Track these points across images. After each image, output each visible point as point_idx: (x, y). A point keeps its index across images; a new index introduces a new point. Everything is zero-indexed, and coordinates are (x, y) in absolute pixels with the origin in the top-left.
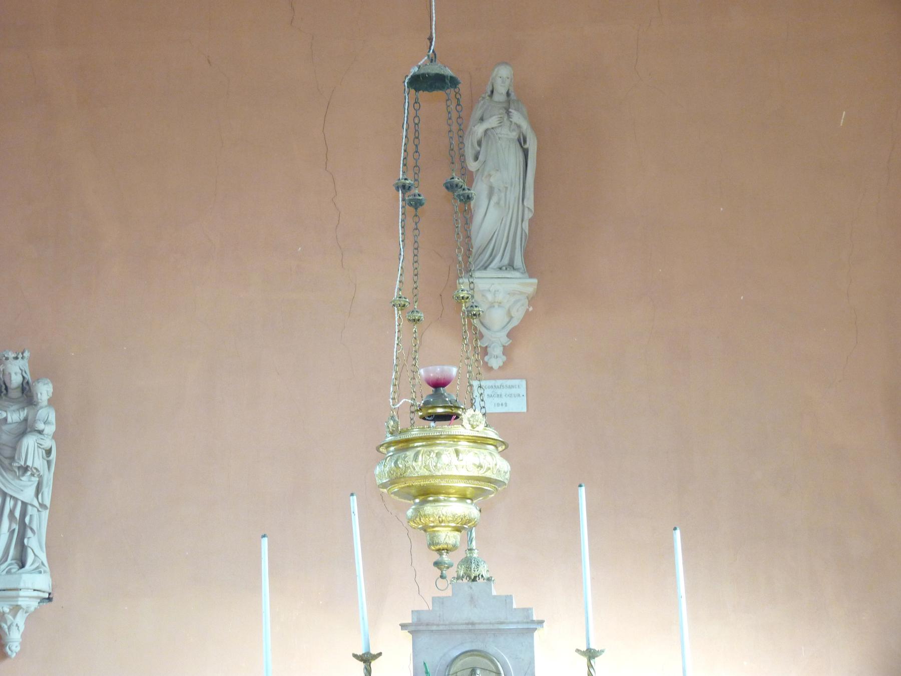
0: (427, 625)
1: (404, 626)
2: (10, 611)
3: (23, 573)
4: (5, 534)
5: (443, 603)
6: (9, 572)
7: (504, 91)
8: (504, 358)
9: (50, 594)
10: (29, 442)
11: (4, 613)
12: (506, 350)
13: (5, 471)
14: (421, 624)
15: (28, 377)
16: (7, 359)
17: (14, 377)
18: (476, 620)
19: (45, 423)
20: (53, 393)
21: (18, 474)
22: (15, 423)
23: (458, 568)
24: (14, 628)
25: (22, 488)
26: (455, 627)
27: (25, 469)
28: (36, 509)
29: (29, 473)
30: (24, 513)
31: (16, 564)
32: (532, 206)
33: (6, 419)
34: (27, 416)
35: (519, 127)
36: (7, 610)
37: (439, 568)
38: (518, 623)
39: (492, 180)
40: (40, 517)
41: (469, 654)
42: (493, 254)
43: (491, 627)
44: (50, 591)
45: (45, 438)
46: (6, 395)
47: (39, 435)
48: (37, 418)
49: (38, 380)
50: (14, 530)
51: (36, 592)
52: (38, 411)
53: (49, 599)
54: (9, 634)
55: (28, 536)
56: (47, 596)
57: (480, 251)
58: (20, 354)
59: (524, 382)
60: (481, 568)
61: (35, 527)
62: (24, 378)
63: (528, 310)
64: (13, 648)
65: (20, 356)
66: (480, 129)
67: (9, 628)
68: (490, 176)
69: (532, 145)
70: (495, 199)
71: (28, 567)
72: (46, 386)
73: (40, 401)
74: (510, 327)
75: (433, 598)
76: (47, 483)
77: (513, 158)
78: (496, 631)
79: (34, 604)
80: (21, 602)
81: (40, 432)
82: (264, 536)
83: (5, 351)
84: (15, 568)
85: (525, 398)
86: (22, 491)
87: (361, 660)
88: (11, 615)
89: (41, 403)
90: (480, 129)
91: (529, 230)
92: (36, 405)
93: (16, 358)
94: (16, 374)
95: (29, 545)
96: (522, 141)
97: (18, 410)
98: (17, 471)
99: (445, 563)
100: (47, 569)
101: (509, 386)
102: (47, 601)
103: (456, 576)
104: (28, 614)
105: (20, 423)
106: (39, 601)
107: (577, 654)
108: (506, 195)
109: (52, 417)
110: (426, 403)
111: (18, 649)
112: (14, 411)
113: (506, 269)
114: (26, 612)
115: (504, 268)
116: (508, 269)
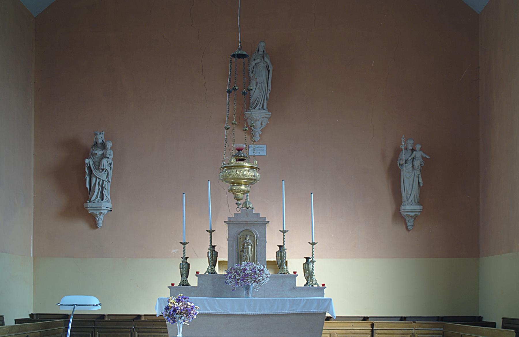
0: (233, 221)
1: (225, 222)
2: (99, 213)
3: (103, 202)
6: (98, 202)
7: (262, 51)
8: (260, 138)
9: (111, 209)
10: (104, 161)
11: (97, 214)
12: (260, 135)
13: (97, 170)
14: (231, 221)
15: (104, 140)
16: (97, 134)
17: (99, 140)
18: (248, 221)
19: (109, 155)
20: (112, 145)
24: (100, 219)
27: (103, 169)
29: (104, 171)
33: (97, 153)
34: (104, 153)
35: (267, 62)
36: (98, 213)
38: (261, 222)
39: (257, 80)
42: (257, 104)
43: (252, 223)
46: (97, 146)
50: (100, 189)
53: (111, 211)
56: (110, 209)
59: (266, 146)
61: (106, 188)
62: (102, 140)
63: (267, 123)
64: (100, 225)
65: (101, 133)
66: (254, 63)
67: (98, 219)
68: (256, 78)
69: (271, 69)
70: (258, 86)
71: (104, 200)
72: (110, 143)
77: (265, 73)
78: (254, 224)
79: (106, 212)
81: (108, 158)
84: (100, 201)
85: (266, 151)
86: (102, 176)
90: (254, 63)
93: (100, 134)
94: (100, 139)
96: (268, 67)
97: (101, 151)
98: (100, 170)
100: (110, 201)
105: (101, 155)
106: (108, 211)
109: (112, 153)
111: (101, 225)
113: (261, 109)
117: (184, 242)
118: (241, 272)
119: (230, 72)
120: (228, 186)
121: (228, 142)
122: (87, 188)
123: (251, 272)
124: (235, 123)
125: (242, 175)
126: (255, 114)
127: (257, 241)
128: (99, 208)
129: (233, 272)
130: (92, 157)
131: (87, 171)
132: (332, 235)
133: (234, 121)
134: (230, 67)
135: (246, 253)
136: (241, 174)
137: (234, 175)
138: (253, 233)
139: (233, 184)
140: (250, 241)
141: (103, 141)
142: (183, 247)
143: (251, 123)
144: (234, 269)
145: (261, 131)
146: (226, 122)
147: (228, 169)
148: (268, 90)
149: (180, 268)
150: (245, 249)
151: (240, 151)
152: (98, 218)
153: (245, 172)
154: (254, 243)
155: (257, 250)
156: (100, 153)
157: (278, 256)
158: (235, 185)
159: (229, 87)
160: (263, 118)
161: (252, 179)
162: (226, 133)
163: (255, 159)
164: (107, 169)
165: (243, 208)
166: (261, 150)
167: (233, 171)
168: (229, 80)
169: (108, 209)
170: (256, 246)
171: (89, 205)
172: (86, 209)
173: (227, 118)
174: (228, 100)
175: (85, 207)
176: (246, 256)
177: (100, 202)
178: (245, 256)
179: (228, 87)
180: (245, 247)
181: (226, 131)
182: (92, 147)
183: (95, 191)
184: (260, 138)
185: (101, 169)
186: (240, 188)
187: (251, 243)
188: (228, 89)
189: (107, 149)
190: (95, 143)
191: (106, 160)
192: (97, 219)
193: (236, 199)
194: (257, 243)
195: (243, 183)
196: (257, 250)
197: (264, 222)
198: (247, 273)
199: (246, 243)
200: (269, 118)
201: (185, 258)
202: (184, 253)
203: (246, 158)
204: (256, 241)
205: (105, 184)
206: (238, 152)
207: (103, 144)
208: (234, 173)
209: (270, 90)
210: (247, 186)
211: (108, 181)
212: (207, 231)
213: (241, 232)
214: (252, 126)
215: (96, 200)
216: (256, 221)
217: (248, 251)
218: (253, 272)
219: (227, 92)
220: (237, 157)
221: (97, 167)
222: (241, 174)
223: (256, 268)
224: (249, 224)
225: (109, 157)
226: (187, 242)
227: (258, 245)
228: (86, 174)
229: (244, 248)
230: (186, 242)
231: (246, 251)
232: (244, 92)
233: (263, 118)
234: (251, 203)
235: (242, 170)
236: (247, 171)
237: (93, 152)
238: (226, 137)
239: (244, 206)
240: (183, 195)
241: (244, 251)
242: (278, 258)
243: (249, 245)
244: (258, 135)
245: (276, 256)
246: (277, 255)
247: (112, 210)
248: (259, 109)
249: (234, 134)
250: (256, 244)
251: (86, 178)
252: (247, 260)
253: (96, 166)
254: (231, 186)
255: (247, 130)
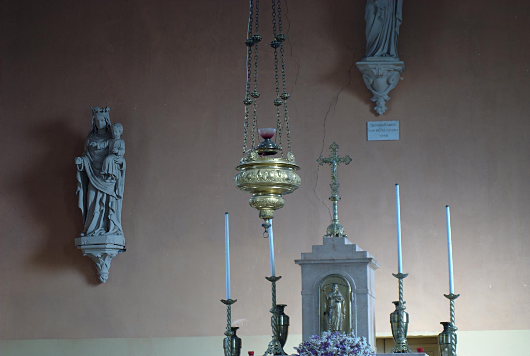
0: (309, 260)
1: (296, 261)
2: (102, 256)
3: (108, 235)
4: (97, 213)
5: (318, 249)
6: (100, 234)
8: (386, 108)
9: (124, 247)
10: (110, 159)
11: (98, 257)
12: (388, 103)
13: (97, 176)
14: (306, 260)
15: (109, 122)
16: (97, 112)
17: (101, 122)
18: (336, 258)
19: (118, 149)
20: (123, 132)
21: (104, 178)
22: (102, 149)
23: (327, 230)
24: (104, 266)
25: (106, 186)
26: (324, 262)
27: (108, 175)
28: (115, 199)
29: (110, 178)
30: (108, 201)
31: (104, 230)
32: (401, 18)
33: (96, 147)
34: (109, 145)
37: (264, 227)
38: (358, 259)
40: (117, 203)
41: (331, 276)
42: (378, 47)
43: (343, 261)
44: (125, 245)
45: (119, 158)
46: (97, 133)
47: (115, 156)
48: (114, 146)
49: (114, 124)
50: (103, 210)
51: (116, 246)
52: (114, 142)
53: (124, 250)
54: (102, 269)
55: (111, 214)
56: (122, 248)
57: (371, 44)
58: (104, 109)
59: (398, 122)
60: (340, 229)
61: (114, 209)
62: (107, 123)
63: (400, 79)
64: (104, 277)
65: (104, 110)
67: (101, 266)
70: (378, 14)
72: (119, 128)
73: (116, 136)
74: (389, 90)
75: (313, 246)
76: (121, 184)
78: (346, 264)
79: (115, 253)
80: (107, 251)
81: (116, 154)
82: (226, 213)
83: (96, 107)
84: (103, 232)
85: (398, 131)
86: (107, 188)
87: (270, 280)
88: (102, 259)
89: (116, 137)
91: (400, 33)
92: (114, 139)
93: (102, 112)
94: (102, 120)
95: (111, 219)
97: (104, 141)
98: (103, 176)
99: (267, 225)
100: (122, 233)
101: (389, 125)
102: (123, 251)
103: (326, 234)
104: (112, 258)
105: (105, 149)
106: (118, 251)
107: (393, 277)
108: (385, 13)
109: (123, 146)
110: (261, 146)
111: (107, 278)
112: (101, 142)
113: (385, 56)
114: (111, 257)
115: (384, 55)
116: (387, 56)
117: (228, 300)
118: (319, 350)
119: (250, 12)
120: (250, 197)
121: (249, 126)
122: (81, 209)
123: (335, 348)
124: (256, 94)
125: (268, 178)
126: (375, 66)
127: (352, 293)
128: (101, 246)
129: (307, 350)
130: (88, 154)
131: (80, 180)
132: (525, 285)
133: (255, 92)
134: (251, 4)
135: (334, 317)
136: (265, 177)
137: (255, 179)
138: (344, 280)
139: (256, 194)
140: (340, 295)
141: (108, 125)
142: (227, 308)
143: (283, 94)
144: (309, 345)
145: (389, 95)
146: (246, 93)
147: (246, 170)
148: (398, 21)
149: (224, 348)
150: (331, 310)
151: (268, 139)
152: (101, 264)
153: (272, 173)
154: (347, 298)
155: (352, 311)
156: (101, 145)
157: (394, 321)
158: (260, 194)
159: (249, 36)
160: (389, 71)
161: (285, 185)
162: (246, 111)
163: (290, 151)
164: (116, 175)
165: (327, 235)
166: (390, 130)
167: (253, 173)
168: (250, 25)
169: (119, 247)
170: (350, 303)
171: (84, 240)
172: (78, 248)
173: (247, 86)
174: (248, 57)
175: (76, 244)
176: (333, 322)
177: (103, 235)
178: (331, 322)
179: (248, 37)
180: (332, 305)
181: (247, 107)
182: (89, 136)
183: (94, 216)
184: (386, 108)
185: (105, 175)
186: (267, 199)
187: (342, 298)
188: (248, 39)
189: (115, 137)
190: (94, 128)
191: (113, 158)
192: (99, 265)
193: (262, 217)
194: (353, 299)
195: (272, 191)
196: (353, 310)
197: (363, 259)
198: (330, 350)
199: (333, 298)
200: (403, 71)
201: (230, 328)
202: (229, 319)
203: (277, 151)
204: (351, 294)
205: (112, 202)
206: (265, 141)
207: (108, 129)
208: (255, 176)
209: (401, 19)
210: (279, 195)
211: (118, 196)
212: (267, 278)
213: (325, 278)
214: (284, 98)
215: (96, 231)
216: (350, 258)
217: (337, 312)
218: (339, 349)
219: (247, 44)
220: (262, 149)
221: (97, 171)
222: (265, 177)
223: (347, 342)
224: (338, 263)
225: (117, 153)
226: (234, 299)
227: (354, 301)
228: (78, 183)
229: (329, 308)
230: (232, 300)
231: (332, 312)
232: (274, 43)
233: (389, 71)
234: (342, 227)
235: (267, 169)
236: (276, 172)
237: (90, 145)
238: (246, 117)
239: (329, 233)
240: (226, 215)
241: (331, 313)
242: (393, 324)
243: (338, 302)
244: (382, 103)
245: (391, 322)
246: (392, 320)
247: (127, 250)
248: (382, 56)
249: (254, 112)
250: (351, 299)
251: (79, 192)
252: (336, 329)
253: (94, 168)
254: (253, 196)
255: (280, 104)
